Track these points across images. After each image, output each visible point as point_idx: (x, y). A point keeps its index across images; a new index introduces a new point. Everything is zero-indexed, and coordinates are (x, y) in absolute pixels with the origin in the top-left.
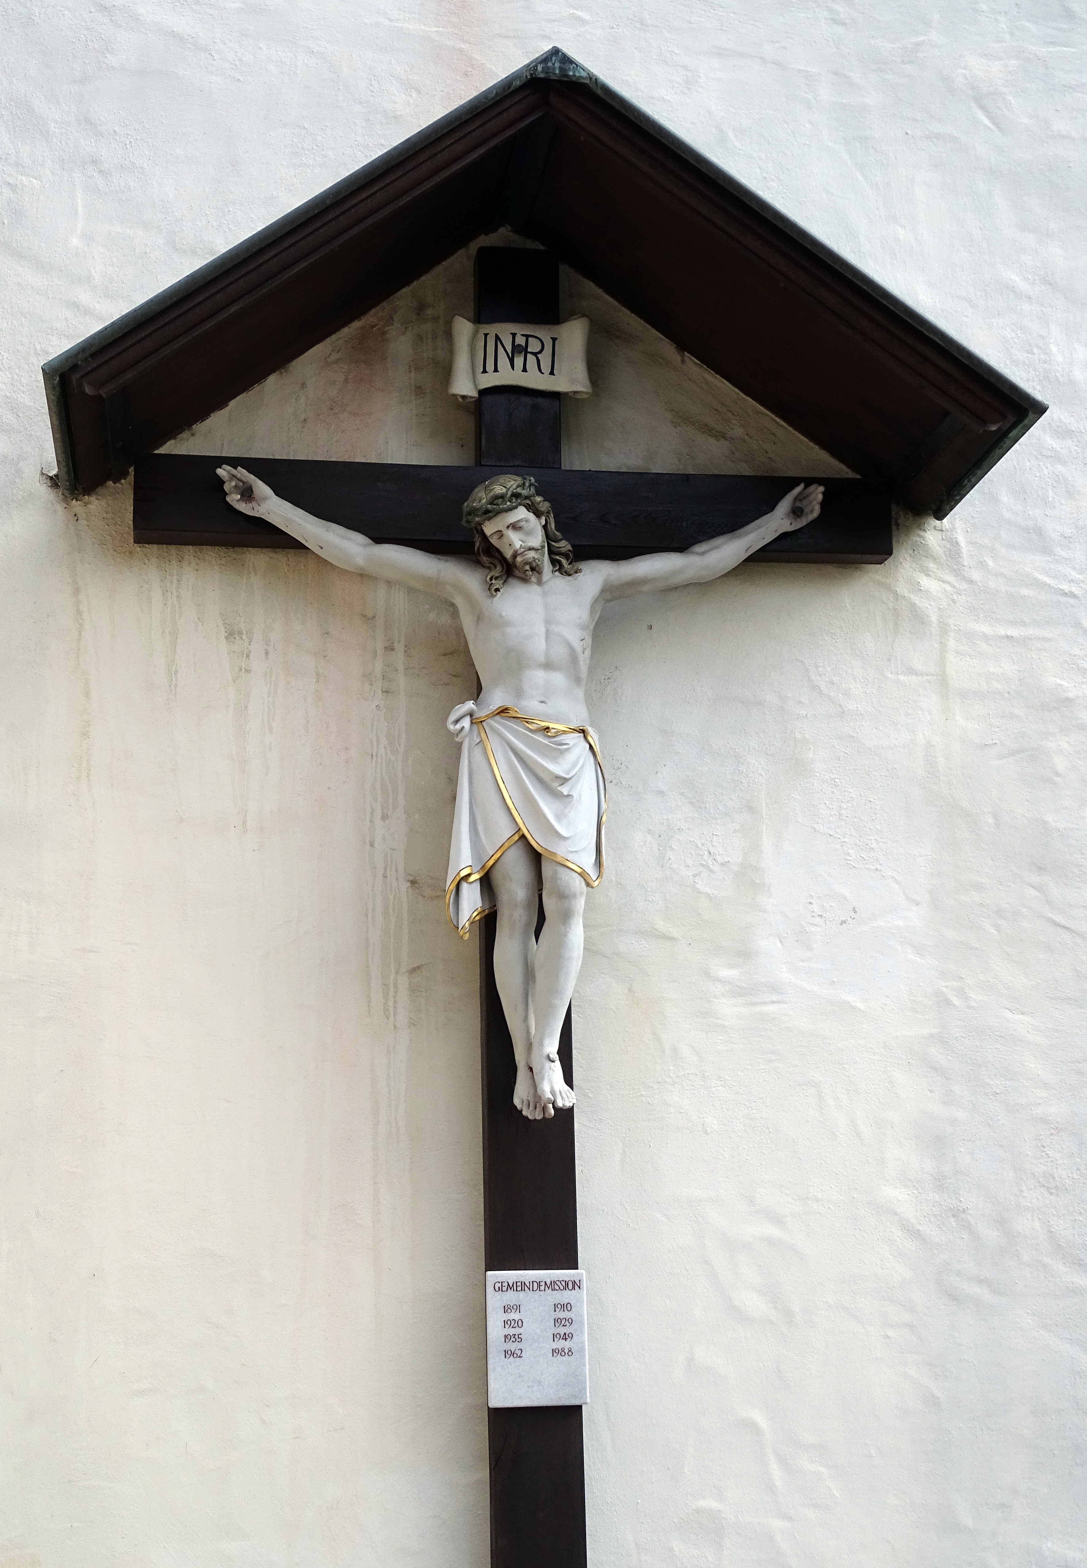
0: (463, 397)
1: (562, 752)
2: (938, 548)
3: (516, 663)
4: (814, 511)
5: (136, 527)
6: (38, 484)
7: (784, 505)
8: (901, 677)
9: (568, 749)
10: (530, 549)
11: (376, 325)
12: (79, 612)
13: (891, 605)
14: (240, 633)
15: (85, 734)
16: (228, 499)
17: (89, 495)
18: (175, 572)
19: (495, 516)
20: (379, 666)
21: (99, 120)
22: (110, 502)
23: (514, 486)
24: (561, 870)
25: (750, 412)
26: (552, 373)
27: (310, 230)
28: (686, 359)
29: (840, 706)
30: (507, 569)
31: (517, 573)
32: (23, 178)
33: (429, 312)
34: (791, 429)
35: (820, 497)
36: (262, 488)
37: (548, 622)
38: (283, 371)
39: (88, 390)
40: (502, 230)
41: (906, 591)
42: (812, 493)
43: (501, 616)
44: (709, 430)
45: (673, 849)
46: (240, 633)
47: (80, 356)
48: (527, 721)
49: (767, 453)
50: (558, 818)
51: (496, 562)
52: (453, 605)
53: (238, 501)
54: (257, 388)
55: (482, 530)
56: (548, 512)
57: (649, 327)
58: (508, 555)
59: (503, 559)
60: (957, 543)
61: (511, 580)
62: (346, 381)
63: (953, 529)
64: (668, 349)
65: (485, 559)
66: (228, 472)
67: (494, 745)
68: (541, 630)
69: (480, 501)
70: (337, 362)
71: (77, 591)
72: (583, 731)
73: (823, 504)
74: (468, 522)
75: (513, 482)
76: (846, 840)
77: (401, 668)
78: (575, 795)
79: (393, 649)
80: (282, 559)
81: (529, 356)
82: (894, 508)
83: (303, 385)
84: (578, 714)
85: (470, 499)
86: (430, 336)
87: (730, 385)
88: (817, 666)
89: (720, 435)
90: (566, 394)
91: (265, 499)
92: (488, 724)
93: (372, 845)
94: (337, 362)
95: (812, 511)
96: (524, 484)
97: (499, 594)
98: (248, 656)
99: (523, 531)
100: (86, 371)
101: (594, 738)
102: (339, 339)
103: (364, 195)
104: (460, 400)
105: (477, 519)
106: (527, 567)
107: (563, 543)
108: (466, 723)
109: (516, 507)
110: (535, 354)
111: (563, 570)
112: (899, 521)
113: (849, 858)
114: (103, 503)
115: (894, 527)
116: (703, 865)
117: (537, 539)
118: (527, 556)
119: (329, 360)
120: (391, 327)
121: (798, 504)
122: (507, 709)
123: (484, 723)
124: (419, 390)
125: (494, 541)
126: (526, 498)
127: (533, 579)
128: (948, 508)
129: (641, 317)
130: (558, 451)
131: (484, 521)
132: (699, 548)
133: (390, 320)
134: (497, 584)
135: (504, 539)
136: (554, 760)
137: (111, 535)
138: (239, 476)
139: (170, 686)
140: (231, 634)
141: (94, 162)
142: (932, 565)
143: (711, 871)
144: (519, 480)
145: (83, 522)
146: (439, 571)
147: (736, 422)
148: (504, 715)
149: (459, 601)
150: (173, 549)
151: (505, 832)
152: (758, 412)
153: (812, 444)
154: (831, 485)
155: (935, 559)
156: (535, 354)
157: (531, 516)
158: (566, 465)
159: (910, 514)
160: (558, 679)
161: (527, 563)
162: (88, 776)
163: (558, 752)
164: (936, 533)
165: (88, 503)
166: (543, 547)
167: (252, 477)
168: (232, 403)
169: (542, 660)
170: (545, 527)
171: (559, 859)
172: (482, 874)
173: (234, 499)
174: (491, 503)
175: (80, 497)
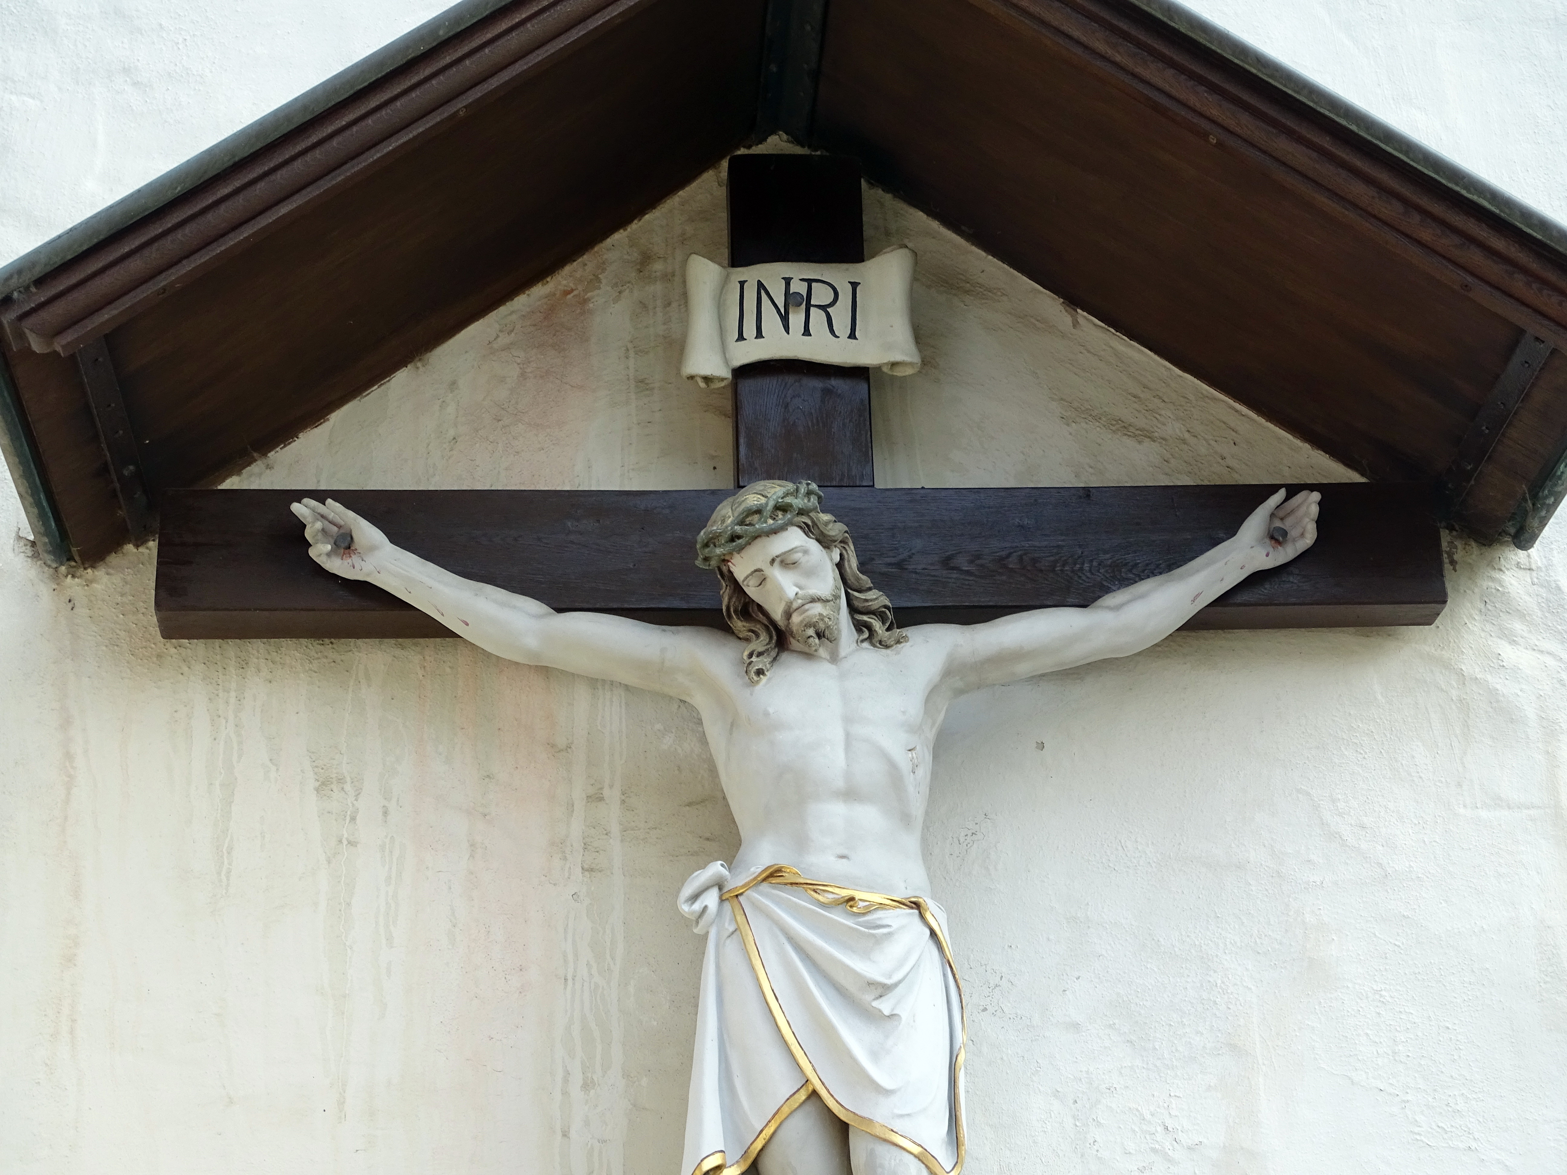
0: (707, 379)
1: (879, 941)
2: (1527, 598)
3: (795, 790)
4: (1305, 533)
5: (159, 605)
6: (11, 555)
7: (1254, 525)
8: (1484, 814)
9: (890, 934)
10: (814, 600)
11: (572, 291)
12: (69, 756)
13: (1454, 693)
14: (341, 780)
15: (69, 960)
16: (312, 553)
17: (93, 567)
18: (233, 685)
19: (749, 543)
20: (576, 828)
21: (137, 11)
22: (129, 578)
23: (781, 494)
24: (882, 1150)
25: (1191, 397)
26: (852, 336)
27: (415, 79)
28: (1081, 320)
29: (1380, 865)
31: (794, 644)
32: (14, 98)
33: (658, 267)
34: (1261, 420)
35: (1314, 510)
36: (367, 533)
37: (848, 720)
38: (419, 364)
39: (37, 345)
40: (773, 140)
41: (1477, 670)
42: (1299, 506)
43: (766, 714)
44: (1122, 427)
45: (1099, 1124)
46: (341, 780)
47: (14, 282)
48: (815, 887)
49: (1223, 458)
50: (875, 1056)
51: (758, 628)
52: (692, 708)
53: (329, 555)
54: (375, 393)
57: (1015, 272)
58: (777, 614)
59: (772, 626)
60: (1558, 588)
62: (523, 375)
63: (1549, 566)
64: (1049, 305)
65: (739, 625)
66: (313, 510)
67: (760, 932)
68: (836, 733)
69: (723, 521)
70: (507, 348)
71: (66, 723)
72: (917, 905)
73: (1320, 522)
74: (706, 559)
75: (778, 488)
76: (1409, 1097)
77: (615, 829)
78: (904, 1016)
79: (601, 799)
80: (414, 656)
81: (812, 309)
82: (1445, 538)
83: (453, 385)
84: (911, 879)
85: (709, 523)
86: (659, 303)
87: (1156, 357)
88: (1334, 801)
89: (1144, 435)
90: (878, 368)
91: (373, 548)
92: (748, 898)
93: (565, 1135)
94: (507, 348)
95: (1302, 535)
96: (797, 490)
98: (353, 819)
99: (797, 570)
100: (27, 308)
101: (937, 916)
102: (512, 312)
103: (504, 25)
104: (702, 385)
105: (718, 551)
106: (811, 632)
107: (873, 594)
108: (711, 899)
109: (783, 528)
110: (823, 308)
112: (1456, 557)
113: (1417, 1130)
114: (117, 579)
115: (1447, 566)
116: (1154, 1150)
117: (826, 582)
118: (810, 613)
119: (495, 346)
120: (597, 292)
121: (1278, 524)
122: (779, 870)
123: (741, 898)
124: (642, 385)
125: (752, 591)
126: (801, 512)
127: (823, 652)
128: (1536, 523)
129: (1003, 261)
130: (867, 458)
131: (731, 553)
132: (1110, 600)
133: (594, 282)
134: (759, 663)
135: (768, 585)
136: (866, 954)
137: (128, 631)
138: (331, 516)
139: (219, 873)
140: (325, 785)
141: (126, 71)
142: (1518, 626)
143: (1170, 1160)
144: (790, 486)
145: (82, 611)
146: (663, 650)
147: (1169, 414)
148: (774, 881)
149: (700, 700)
150: (231, 647)
151: (781, 1087)
152: (1205, 397)
153: (1298, 443)
154: (1332, 495)
155: (1522, 616)
156: (823, 308)
157: (813, 545)
159: (1473, 544)
160: (869, 816)
161: (809, 625)
162: (72, 1032)
163: (873, 940)
164: (1520, 574)
165: (91, 581)
166: (837, 597)
167: (351, 514)
168: (335, 417)
169: (840, 783)
170: (840, 566)
171: (878, 1131)
172: (744, 1167)
173: (320, 552)
174: (742, 523)
175: (81, 571)
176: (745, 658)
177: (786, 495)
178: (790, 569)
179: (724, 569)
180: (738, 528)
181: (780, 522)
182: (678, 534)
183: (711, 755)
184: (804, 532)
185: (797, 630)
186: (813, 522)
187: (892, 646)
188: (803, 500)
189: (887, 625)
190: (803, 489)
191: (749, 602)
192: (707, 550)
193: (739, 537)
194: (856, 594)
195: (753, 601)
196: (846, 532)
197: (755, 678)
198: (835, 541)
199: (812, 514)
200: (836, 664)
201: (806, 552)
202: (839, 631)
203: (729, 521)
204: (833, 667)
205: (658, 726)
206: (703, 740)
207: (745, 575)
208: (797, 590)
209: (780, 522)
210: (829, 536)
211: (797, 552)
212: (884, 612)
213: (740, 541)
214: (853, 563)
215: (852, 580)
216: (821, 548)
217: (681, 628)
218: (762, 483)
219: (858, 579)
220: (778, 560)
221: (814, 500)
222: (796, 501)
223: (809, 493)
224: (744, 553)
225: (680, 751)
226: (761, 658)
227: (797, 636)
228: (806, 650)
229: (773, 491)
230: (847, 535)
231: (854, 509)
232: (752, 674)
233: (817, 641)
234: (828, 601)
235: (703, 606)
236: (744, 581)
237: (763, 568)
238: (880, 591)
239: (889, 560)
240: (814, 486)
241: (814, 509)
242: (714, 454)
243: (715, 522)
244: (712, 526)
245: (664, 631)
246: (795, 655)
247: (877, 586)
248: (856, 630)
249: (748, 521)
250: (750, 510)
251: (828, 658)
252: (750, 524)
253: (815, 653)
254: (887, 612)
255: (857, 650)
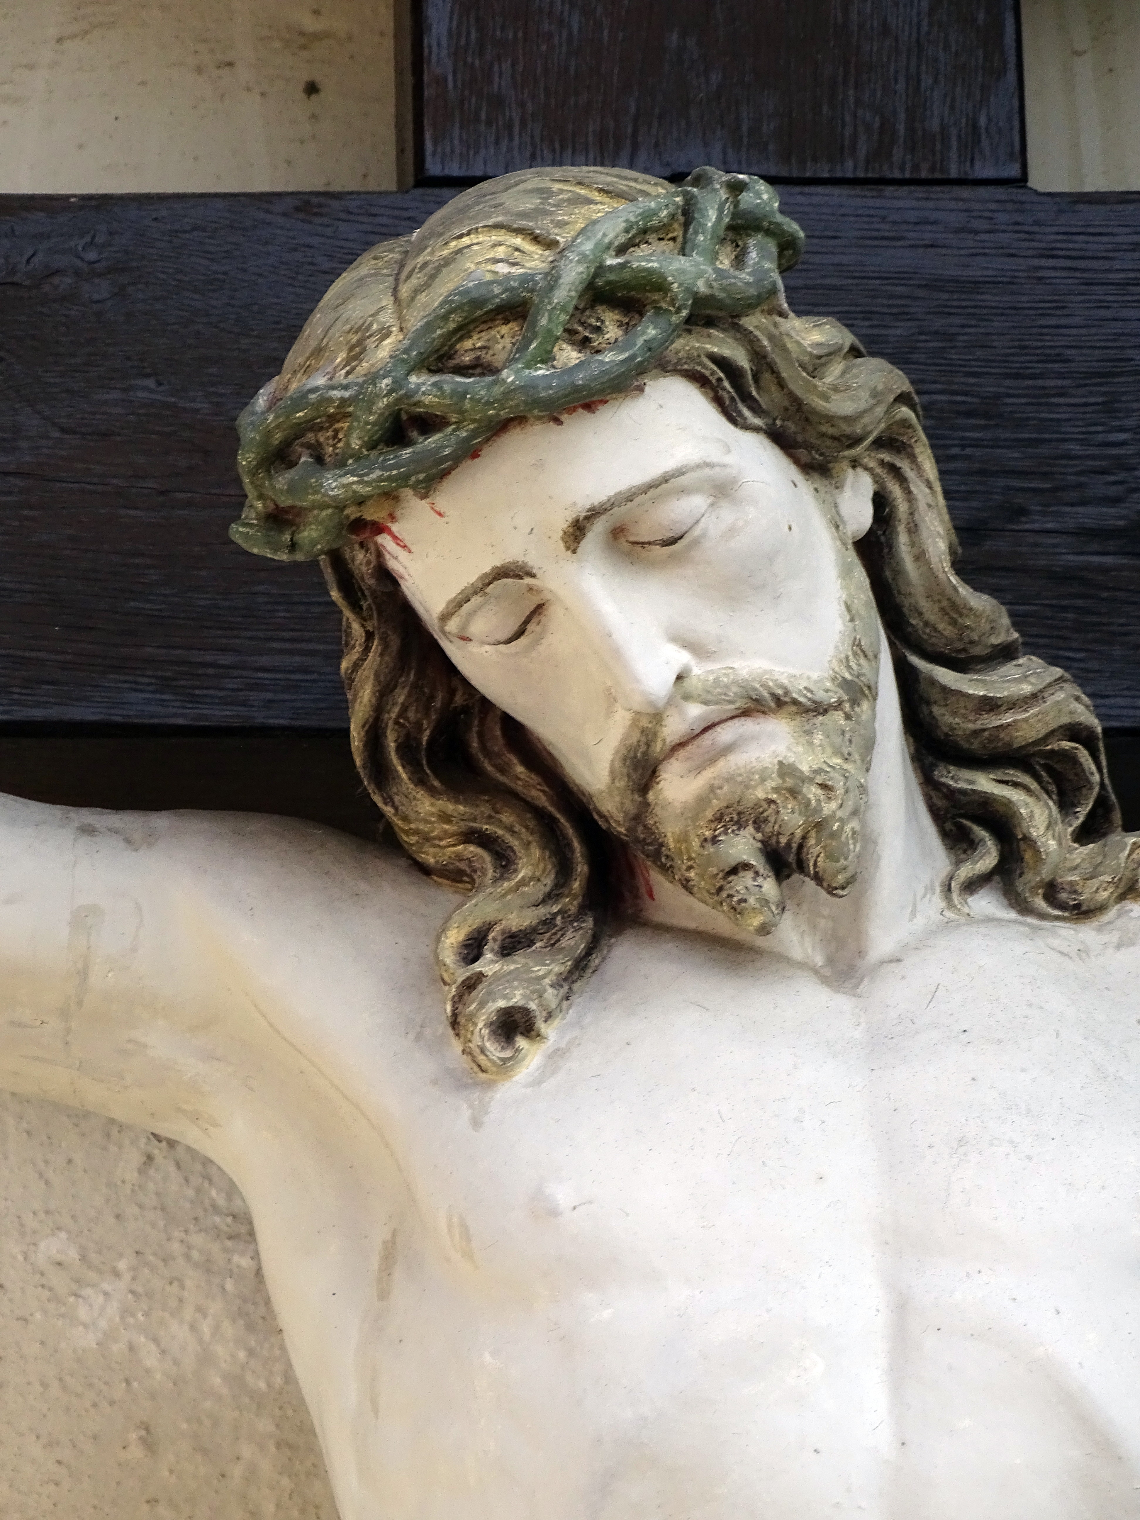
10: (762, 703)
19: (469, 452)
23: (613, 230)
30: (601, 875)
31: (669, 899)
37: (904, 1245)
51: (506, 824)
55: (387, 578)
56: (891, 442)
58: (594, 762)
59: (564, 814)
61: (628, 957)
65: (423, 810)
68: (852, 1300)
69: (357, 352)
74: (279, 519)
75: (603, 206)
85: (295, 357)
96: (688, 214)
97: (532, 1056)
105: (336, 484)
106: (743, 846)
107: (1022, 677)
109: (623, 384)
111: (1029, 880)
117: (810, 623)
118: (738, 761)
125: (481, 660)
126: (706, 313)
127: (794, 937)
131: (390, 496)
134: (510, 983)
135: (557, 637)
144: (658, 196)
146: (84, 919)
149: (244, 1143)
157: (754, 460)
158: (1048, 174)
161: (733, 817)
166: (858, 691)
170: (874, 551)
174: (439, 359)
176: (449, 957)
177: (640, 234)
178: (653, 565)
179: (360, 560)
180: (422, 384)
181: (608, 357)
182: (146, 390)
183: (289, 1377)
184: (718, 401)
185: (684, 838)
186: (758, 356)
187: (1101, 908)
188: (714, 257)
189: (1083, 811)
190: (712, 214)
191: (466, 710)
192: (282, 481)
193: (430, 423)
194: (945, 676)
195: (486, 705)
196: (903, 399)
197: (495, 1050)
198: (856, 441)
199: (751, 322)
200: (854, 992)
201: (723, 490)
202: (867, 839)
203: (383, 352)
204: (842, 1002)
205: (52, 1247)
206: (256, 1310)
207: (453, 591)
208: (682, 658)
209: (608, 357)
210: (830, 419)
211: (683, 491)
212: (1069, 758)
213: (433, 441)
214: (931, 536)
215: (930, 611)
216: (793, 472)
217: (161, 821)
218: (532, 179)
219: (954, 609)
220: (598, 529)
221: (761, 258)
222: (682, 263)
223: (741, 228)
224: (447, 497)
225: (150, 1358)
226: (517, 962)
227: (681, 865)
228: (720, 922)
229: (579, 217)
230: (905, 411)
231: (935, 284)
232: (480, 1030)
233: (769, 886)
234: (819, 709)
235: (261, 717)
236: (445, 617)
237: (533, 560)
238: (1053, 661)
239: (1088, 515)
240: (762, 196)
241: (763, 300)
242: (310, 24)
243: (318, 351)
244: (308, 370)
245: (87, 830)
246: (670, 946)
247: (1041, 636)
248: (945, 835)
249: (468, 348)
250: (476, 303)
251: (819, 960)
252: (479, 368)
253: (761, 942)
254: (1084, 755)
255: (948, 926)
